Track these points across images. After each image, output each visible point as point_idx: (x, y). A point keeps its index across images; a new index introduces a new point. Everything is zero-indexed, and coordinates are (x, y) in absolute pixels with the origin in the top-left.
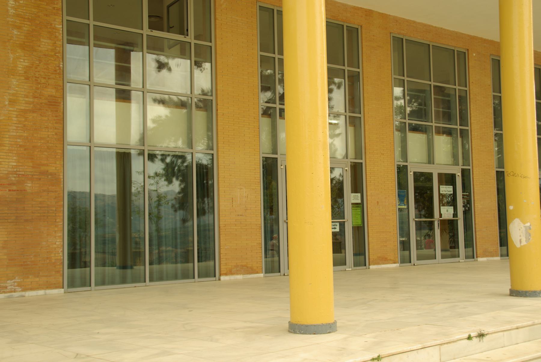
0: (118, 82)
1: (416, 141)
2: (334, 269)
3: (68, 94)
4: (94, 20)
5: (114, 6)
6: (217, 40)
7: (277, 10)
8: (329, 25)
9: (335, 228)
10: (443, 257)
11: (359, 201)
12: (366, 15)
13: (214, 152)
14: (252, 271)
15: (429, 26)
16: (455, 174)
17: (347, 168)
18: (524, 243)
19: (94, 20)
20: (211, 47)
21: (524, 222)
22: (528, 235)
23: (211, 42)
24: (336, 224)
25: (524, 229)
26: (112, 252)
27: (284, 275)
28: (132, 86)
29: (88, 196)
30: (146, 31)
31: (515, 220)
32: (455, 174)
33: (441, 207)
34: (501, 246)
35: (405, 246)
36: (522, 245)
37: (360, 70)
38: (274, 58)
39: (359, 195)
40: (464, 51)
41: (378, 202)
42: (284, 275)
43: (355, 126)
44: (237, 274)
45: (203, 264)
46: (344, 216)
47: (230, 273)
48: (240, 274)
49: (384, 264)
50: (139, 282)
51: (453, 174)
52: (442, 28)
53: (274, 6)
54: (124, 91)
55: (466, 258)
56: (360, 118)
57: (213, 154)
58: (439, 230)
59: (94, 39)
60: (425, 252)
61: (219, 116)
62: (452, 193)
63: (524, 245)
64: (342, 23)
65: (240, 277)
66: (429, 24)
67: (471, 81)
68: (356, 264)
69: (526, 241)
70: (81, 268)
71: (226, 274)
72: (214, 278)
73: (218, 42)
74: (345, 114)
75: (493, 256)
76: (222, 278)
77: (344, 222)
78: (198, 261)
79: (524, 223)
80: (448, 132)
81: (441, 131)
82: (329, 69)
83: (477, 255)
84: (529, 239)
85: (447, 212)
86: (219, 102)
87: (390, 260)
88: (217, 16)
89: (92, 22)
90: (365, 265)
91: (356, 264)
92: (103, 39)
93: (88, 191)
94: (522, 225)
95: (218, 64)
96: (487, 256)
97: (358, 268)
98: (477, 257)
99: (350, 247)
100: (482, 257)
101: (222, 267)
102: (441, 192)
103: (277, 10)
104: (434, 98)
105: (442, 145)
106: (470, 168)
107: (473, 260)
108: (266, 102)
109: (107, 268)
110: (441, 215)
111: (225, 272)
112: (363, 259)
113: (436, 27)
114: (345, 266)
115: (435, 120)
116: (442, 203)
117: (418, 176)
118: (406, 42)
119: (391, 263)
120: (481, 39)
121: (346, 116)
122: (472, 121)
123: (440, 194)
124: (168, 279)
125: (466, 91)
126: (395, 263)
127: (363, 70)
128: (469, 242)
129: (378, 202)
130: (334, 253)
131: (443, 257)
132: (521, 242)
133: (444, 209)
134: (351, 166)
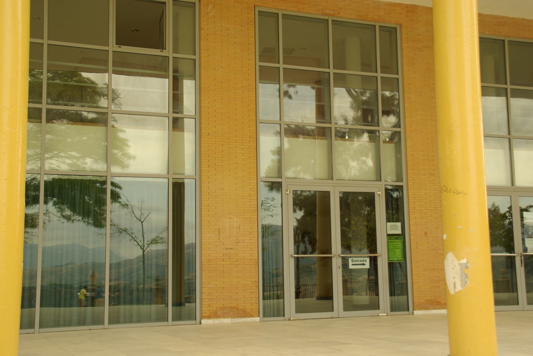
0: (31, 100)
3: (261, 134)
4: (284, 63)
5: (138, 31)
6: (202, 51)
7: (283, 14)
8: (482, 41)
9: (364, 264)
10: (298, 311)
11: (399, 232)
12: (407, 12)
14: (245, 314)
15: (503, 17)
17: (380, 193)
18: (459, 288)
19: (284, 63)
20: (398, 79)
21: (459, 258)
22: (464, 277)
23: (398, 74)
24: (365, 259)
25: (458, 268)
26: (157, 290)
28: (185, 113)
29: (280, 229)
30: (112, 47)
31: (448, 255)
36: (456, 290)
37: (259, 64)
38: (377, 77)
39: (399, 224)
41: (426, 233)
42: (290, 320)
44: (224, 317)
45: (45, 309)
47: (215, 315)
48: (228, 317)
49: (435, 309)
50: (278, 315)
52: (523, 19)
53: (278, 9)
55: (392, 310)
56: (400, 132)
59: (113, 66)
60: (504, 296)
61: (202, 136)
63: (459, 291)
64: (503, 38)
65: (227, 321)
66: (504, 15)
68: (394, 308)
69: (461, 285)
70: (55, 307)
71: (209, 317)
72: (407, 312)
73: (202, 55)
76: (204, 321)
78: (41, 306)
79: (459, 260)
82: (482, 87)
83: (414, 306)
84: (466, 283)
86: (203, 120)
88: (202, 26)
89: (282, 66)
90: (408, 310)
91: (394, 308)
92: (294, 78)
93: (280, 224)
94: (456, 262)
95: (202, 79)
97: (397, 313)
100: (420, 309)
101: (203, 309)
103: (283, 14)
108: (394, 127)
109: (122, 307)
110: (525, 250)
111: (207, 315)
113: (513, 18)
114: (377, 311)
116: (527, 234)
118: (333, 24)
124: (65, 325)
125: (398, 79)
127: (403, 75)
130: (343, 295)
131: (298, 311)
132: (455, 287)
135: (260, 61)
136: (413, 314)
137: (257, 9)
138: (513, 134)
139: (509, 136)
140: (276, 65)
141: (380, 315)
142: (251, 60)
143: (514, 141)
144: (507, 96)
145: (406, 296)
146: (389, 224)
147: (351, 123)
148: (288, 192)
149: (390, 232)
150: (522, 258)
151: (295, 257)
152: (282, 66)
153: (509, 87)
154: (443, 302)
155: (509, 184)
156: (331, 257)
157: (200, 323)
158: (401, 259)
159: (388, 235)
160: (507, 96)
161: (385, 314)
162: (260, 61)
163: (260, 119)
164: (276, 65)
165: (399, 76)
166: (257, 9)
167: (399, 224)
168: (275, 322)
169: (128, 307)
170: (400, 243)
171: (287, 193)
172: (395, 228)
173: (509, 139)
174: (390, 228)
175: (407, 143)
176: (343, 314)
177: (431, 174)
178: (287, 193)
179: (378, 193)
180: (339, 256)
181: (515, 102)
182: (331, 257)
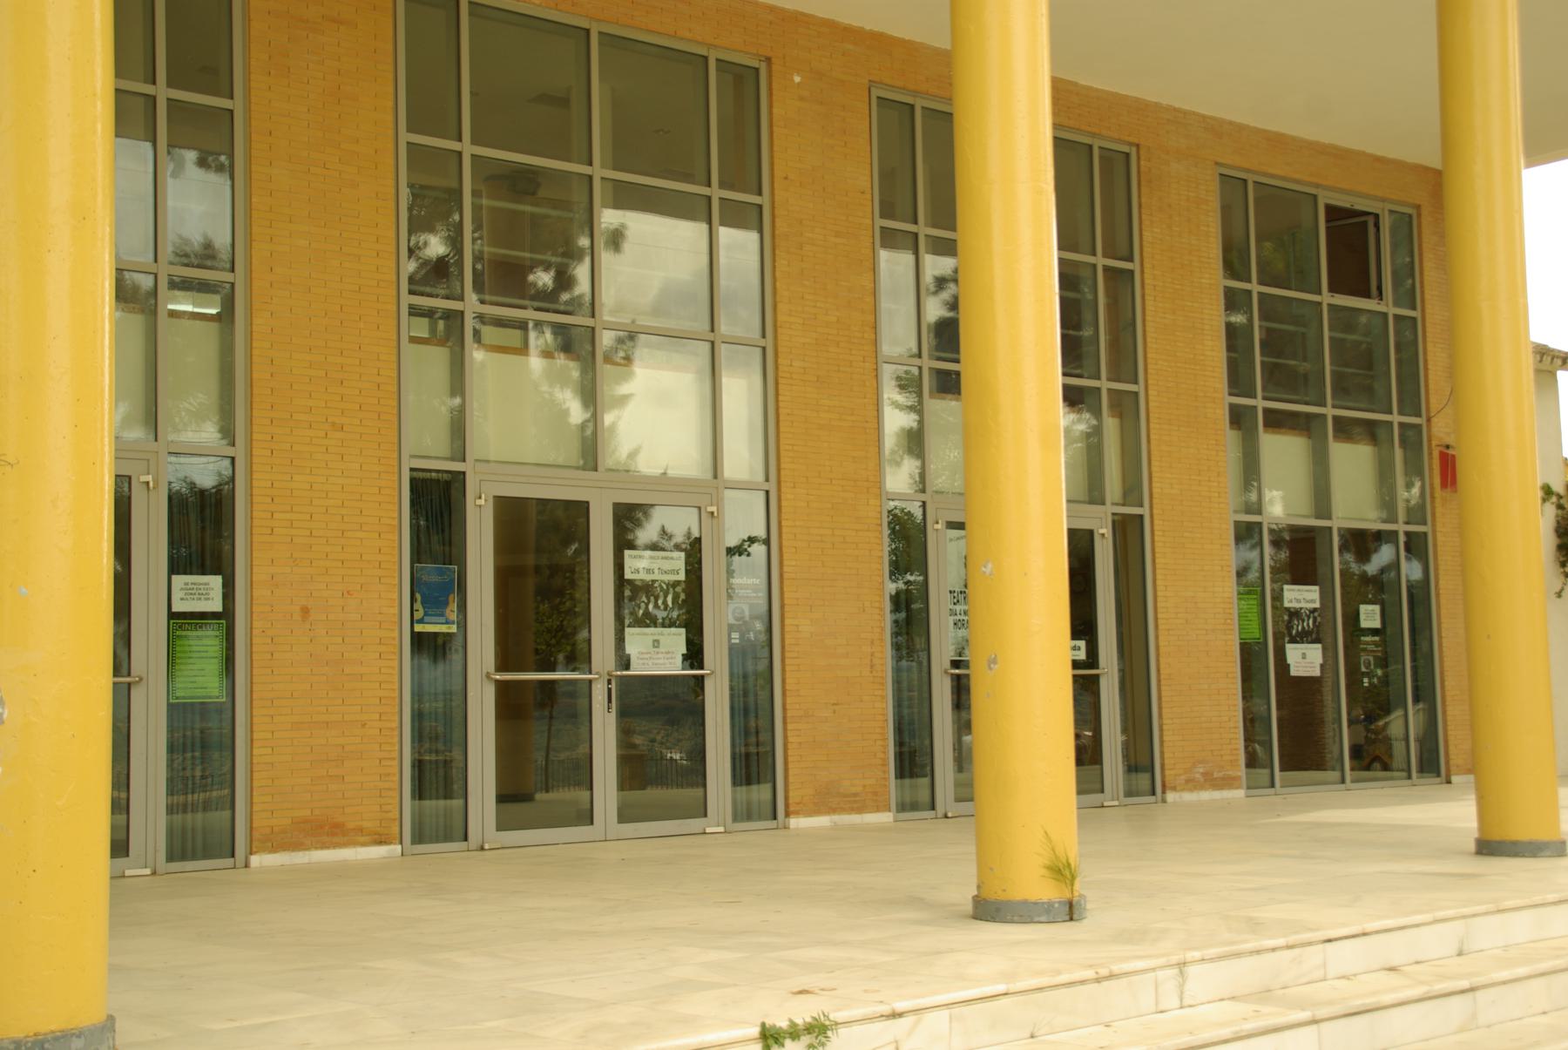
1: (1283, 454)
2: (112, 866)
4: (170, 84)
10: (623, 817)
11: (216, 605)
13: (239, 452)
14: (857, 805)
16: (1091, 532)
17: (149, 478)
19: (170, 84)
20: (760, 207)
27: (482, 849)
32: (1091, 532)
33: (628, 630)
34: (901, 774)
35: (436, 773)
38: (460, 154)
40: (755, 64)
41: (305, 611)
42: (482, 849)
43: (1121, 416)
46: (730, 655)
47: (1192, 785)
50: (448, 838)
51: (568, 504)
54: (948, 373)
56: (1136, 394)
57: (233, 459)
58: (612, 718)
62: (682, 577)
64: (585, 25)
67: (778, 173)
68: (744, 813)
72: (229, 862)
74: (762, 343)
75: (861, 809)
76: (255, 860)
77: (702, 677)
80: (1372, 432)
81: (1345, 430)
83: (787, 805)
85: (657, 653)
87: (360, 830)
89: (468, 148)
90: (775, 818)
96: (832, 810)
98: (787, 815)
99: (1119, 748)
100: (274, 849)
102: (628, 575)
104: (1331, 338)
105: (1352, 463)
106: (1145, 511)
107: (773, 824)
110: (625, 663)
112: (768, 795)
115: (1333, 398)
117: (511, 512)
118: (718, 69)
119: (364, 844)
120: (831, 25)
121: (764, 349)
122: (780, 318)
123: (621, 581)
125: (760, 207)
126: (380, 843)
128: (753, 765)
129: (305, 611)
131: (623, 817)
133: (638, 642)
134: (1114, 522)
135: (409, 130)
136: (1164, 801)
137: (875, 93)
138: (724, 328)
139: (711, 337)
140: (453, 145)
141: (128, 873)
142: (866, 216)
143: (723, 350)
144: (710, 223)
145: (701, 790)
146: (178, 580)
147: (172, 258)
148: (482, 502)
149: (178, 607)
150: (613, 686)
151: (497, 681)
152: (468, 148)
153: (716, 193)
154: (351, 825)
155: (709, 475)
156: (1097, 677)
157: (247, 866)
158: (216, 692)
159: (172, 615)
160: (710, 223)
161: (148, 871)
162: (409, 130)
163: (606, 318)
164: (453, 145)
165: (237, 105)
166: (875, 93)
167: (216, 581)
168: (921, 822)
169: (434, 802)
170: (216, 642)
171: (479, 502)
172: (204, 592)
173: (713, 343)
174: (181, 594)
175: (256, 321)
176: (494, 837)
177: (333, 424)
178: (479, 502)
179: (143, 478)
180: (488, 676)
181: (725, 234)
182: (1097, 677)
